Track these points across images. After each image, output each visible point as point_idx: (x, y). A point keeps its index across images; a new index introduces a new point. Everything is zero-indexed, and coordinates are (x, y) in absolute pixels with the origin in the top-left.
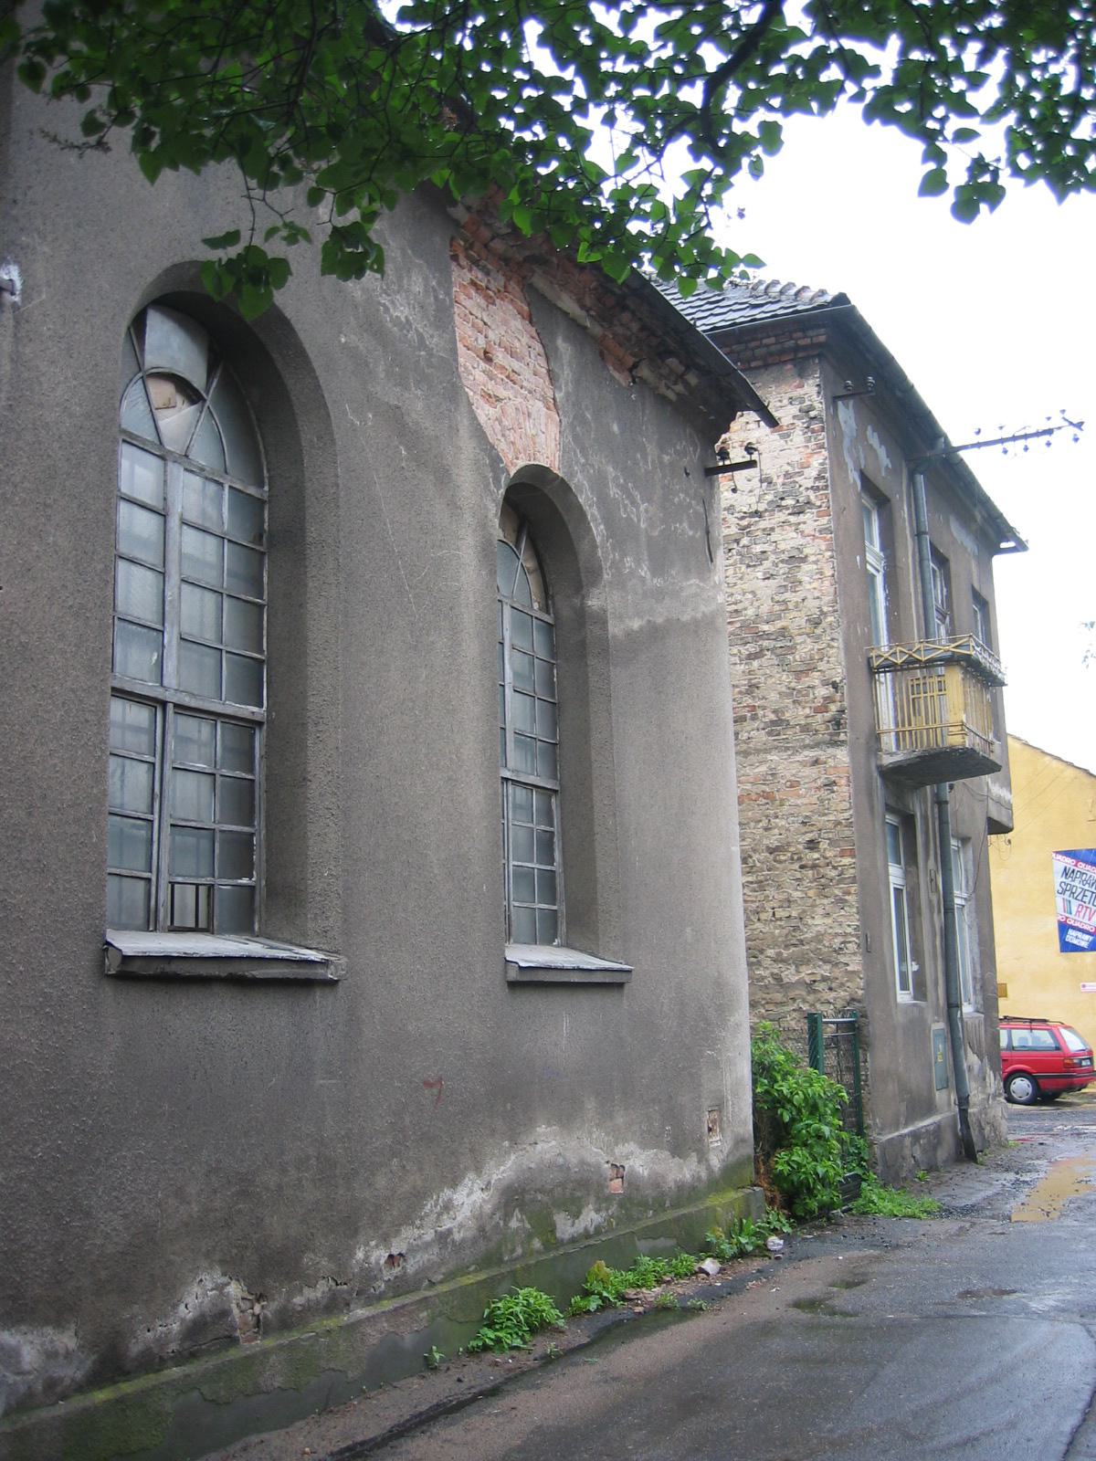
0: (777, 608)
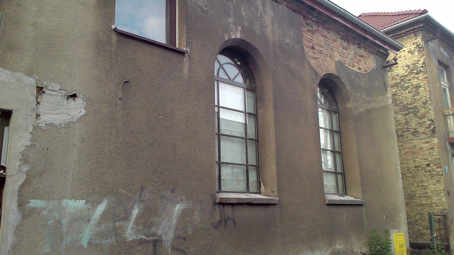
0: (413, 100)
